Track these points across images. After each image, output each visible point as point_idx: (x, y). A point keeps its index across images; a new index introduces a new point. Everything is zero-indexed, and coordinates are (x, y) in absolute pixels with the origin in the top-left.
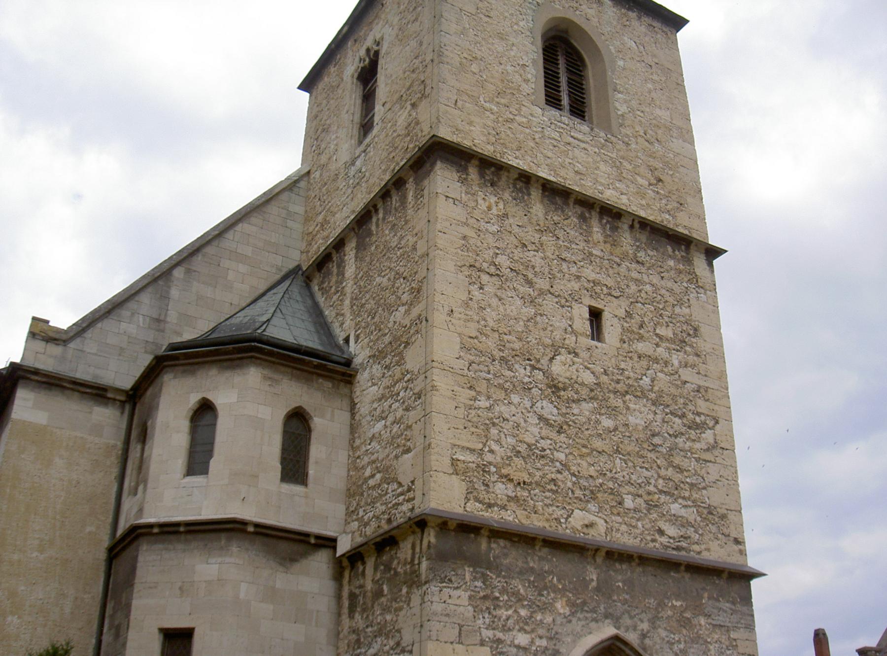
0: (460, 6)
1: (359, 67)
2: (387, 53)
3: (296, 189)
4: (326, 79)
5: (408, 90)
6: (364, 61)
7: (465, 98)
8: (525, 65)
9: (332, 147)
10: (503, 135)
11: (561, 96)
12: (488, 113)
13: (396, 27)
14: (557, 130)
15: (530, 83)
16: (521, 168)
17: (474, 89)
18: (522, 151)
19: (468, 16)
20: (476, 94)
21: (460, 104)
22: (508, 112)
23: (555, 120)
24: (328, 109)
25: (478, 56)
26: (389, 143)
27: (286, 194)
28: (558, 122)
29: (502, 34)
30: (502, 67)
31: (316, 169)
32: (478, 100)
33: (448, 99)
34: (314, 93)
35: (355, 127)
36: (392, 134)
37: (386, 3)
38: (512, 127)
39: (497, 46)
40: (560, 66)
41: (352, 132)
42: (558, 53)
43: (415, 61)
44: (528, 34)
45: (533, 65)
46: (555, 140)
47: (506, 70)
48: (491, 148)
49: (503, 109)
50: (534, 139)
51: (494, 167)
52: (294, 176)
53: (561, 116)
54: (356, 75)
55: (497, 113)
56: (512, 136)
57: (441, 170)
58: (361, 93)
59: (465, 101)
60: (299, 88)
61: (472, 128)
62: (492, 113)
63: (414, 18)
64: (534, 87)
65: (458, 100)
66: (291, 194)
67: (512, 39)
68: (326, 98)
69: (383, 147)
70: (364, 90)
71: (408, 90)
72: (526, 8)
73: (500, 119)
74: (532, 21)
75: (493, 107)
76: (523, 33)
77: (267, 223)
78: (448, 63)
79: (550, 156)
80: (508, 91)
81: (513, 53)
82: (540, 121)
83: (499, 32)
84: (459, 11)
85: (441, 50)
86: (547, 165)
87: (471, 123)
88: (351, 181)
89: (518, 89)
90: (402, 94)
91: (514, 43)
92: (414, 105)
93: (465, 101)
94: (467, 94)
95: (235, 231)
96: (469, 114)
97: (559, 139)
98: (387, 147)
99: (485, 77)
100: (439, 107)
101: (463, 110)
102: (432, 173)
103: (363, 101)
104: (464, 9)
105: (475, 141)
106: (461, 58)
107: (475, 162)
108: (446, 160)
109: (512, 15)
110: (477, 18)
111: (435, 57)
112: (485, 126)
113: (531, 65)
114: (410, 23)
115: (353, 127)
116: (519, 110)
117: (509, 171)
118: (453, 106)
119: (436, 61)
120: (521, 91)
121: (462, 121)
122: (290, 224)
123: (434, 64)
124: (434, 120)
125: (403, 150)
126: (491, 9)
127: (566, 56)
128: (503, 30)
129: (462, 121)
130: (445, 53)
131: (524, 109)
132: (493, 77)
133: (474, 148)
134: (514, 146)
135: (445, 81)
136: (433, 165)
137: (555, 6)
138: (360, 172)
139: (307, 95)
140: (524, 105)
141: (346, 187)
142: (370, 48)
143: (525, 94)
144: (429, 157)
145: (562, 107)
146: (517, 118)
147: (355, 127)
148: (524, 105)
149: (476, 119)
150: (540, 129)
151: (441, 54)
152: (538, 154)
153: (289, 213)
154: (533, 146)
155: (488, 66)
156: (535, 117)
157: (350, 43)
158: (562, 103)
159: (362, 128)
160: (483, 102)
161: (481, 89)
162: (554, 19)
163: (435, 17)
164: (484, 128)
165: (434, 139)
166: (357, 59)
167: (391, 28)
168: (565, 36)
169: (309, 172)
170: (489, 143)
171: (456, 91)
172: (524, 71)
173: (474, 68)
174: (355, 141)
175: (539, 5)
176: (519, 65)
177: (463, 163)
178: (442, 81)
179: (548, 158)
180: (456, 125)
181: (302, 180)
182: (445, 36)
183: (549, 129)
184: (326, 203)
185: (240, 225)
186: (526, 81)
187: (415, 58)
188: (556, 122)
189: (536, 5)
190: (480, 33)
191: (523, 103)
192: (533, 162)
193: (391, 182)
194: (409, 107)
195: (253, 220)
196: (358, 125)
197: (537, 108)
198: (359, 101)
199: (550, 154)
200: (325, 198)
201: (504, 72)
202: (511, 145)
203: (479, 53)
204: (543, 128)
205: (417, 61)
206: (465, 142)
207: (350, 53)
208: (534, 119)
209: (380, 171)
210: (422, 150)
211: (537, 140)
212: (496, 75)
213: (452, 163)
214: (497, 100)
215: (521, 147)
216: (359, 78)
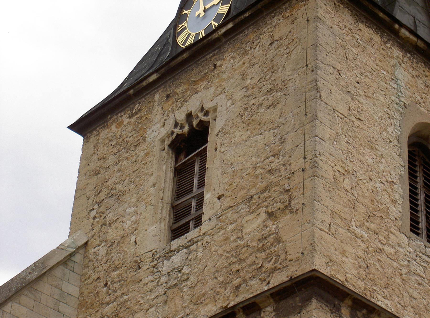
0: (334, 104)
1: (173, 133)
2: (223, 132)
3: (70, 264)
4: (114, 128)
5: (263, 192)
6: (182, 127)
7: (338, 221)
8: (393, 182)
9: (129, 223)
10: (372, 269)
11: (419, 217)
12: (359, 240)
13: (239, 104)
14: (422, 264)
15: (397, 205)
16: (389, 310)
17: (346, 210)
18: (390, 290)
19: (341, 118)
20: (347, 217)
21: (333, 227)
22: (377, 241)
23: (420, 252)
24: (119, 170)
25: (350, 169)
26: (231, 251)
27: (61, 268)
28: (423, 254)
29: (372, 142)
30: (372, 183)
31: (98, 243)
32: (349, 224)
33: (323, 222)
34: (91, 140)
35: (165, 207)
36: (235, 241)
37: (220, 66)
38: (381, 259)
39: (367, 157)
40: (418, 180)
41: (161, 213)
42: (417, 163)
43: (272, 158)
44: (396, 143)
45: (400, 183)
46: (420, 276)
47: (376, 188)
48: (361, 284)
49: (373, 236)
50: (401, 275)
51: (367, 309)
52: (69, 247)
53: (425, 246)
54: (168, 141)
55: (367, 241)
56: (380, 269)
57: (316, 310)
58: (173, 165)
59: (339, 226)
60: (72, 127)
61: (345, 259)
62: (363, 241)
63: (270, 103)
64: (401, 210)
65: (332, 224)
66: (66, 269)
67: (381, 149)
68: (115, 154)
69: (220, 252)
70: (176, 161)
71: (263, 192)
72: (394, 109)
73: (370, 249)
74: (400, 127)
75: (364, 234)
76: (391, 142)
77: (38, 303)
78: (322, 176)
79: (415, 297)
80: (378, 214)
81: (382, 168)
82: (406, 252)
83: (369, 139)
84: (332, 111)
85: (317, 160)
86: (412, 307)
87: (343, 253)
88: (164, 279)
89: (387, 213)
90: (251, 193)
91: (384, 153)
92: (271, 215)
93: (339, 226)
94: (340, 216)
95: (3, 311)
96: (341, 241)
97: (424, 276)
98: (228, 255)
99: (356, 196)
100: (314, 232)
101: (336, 236)
102: (304, 311)
103: (174, 175)
104: (337, 109)
105: (347, 275)
106: (334, 171)
107: (349, 302)
108: (321, 298)
109: (381, 118)
110: (348, 121)
111: (307, 166)
112: (357, 257)
113: (398, 182)
114: (264, 107)
115: (163, 207)
116: (387, 238)
117: (379, 315)
118: (327, 231)
119: (309, 172)
120: (389, 215)
121: (335, 250)
122: (63, 307)
123: (307, 175)
124: (306, 244)
125: (254, 267)
126: (362, 110)
127: (425, 167)
128: (373, 137)
129: (335, 250)
130: (320, 164)
131: (392, 237)
132: (364, 196)
133: (346, 283)
134: (383, 283)
135: (320, 200)
136: (306, 301)
137: (421, 108)
138: (180, 272)
139: (79, 139)
140: (392, 233)
141: (155, 283)
142: (194, 114)
143: (393, 218)
144: (299, 290)
145: (419, 232)
146: (386, 248)
147: (165, 207)
148: (392, 233)
149: (347, 248)
150: (406, 263)
151: (316, 165)
152: (405, 294)
153: (62, 293)
154: (400, 283)
155: (360, 182)
156: (402, 247)
157: (157, 97)
158: (420, 226)
159: (172, 209)
160: (354, 227)
161: (353, 210)
162: (419, 124)
163: (306, 115)
164: (356, 260)
165: (313, 273)
166: (171, 122)
167: (230, 101)
168: (424, 142)
169: (86, 244)
170: (360, 279)
171: (330, 212)
172: (392, 189)
173: (347, 184)
174: (165, 226)
175: (405, 107)
176: (387, 182)
177: (336, 303)
178: (317, 199)
179: (414, 298)
180: (330, 254)
181: (78, 252)
182: (320, 143)
183: (414, 262)
184: (119, 293)
185: (10, 304)
186: (394, 202)
187: (273, 156)
188: (421, 255)
189: (403, 107)
190: (351, 139)
191: (391, 229)
192: (400, 304)
193: (241, 306)
194: (264, 216)
195: (24, 299)
196: (169, 206)
197: (404, 236)
198: (170, 175)
199: (415, 294)
200: (116, 286)
201: (375, 190)
202: (380, 281)
203: (351, 165)
204: (409, 261)
205: (277, 161)
206: (338, 276)
207: (157, 109)
208: (401, 250)
209: (215, 281)
210: (294, 281)
211: (404, 276)
212: (367, 194)
213: (327, 302)
214: (367, 224)
215: (389, 284)
216: (172, 146)
